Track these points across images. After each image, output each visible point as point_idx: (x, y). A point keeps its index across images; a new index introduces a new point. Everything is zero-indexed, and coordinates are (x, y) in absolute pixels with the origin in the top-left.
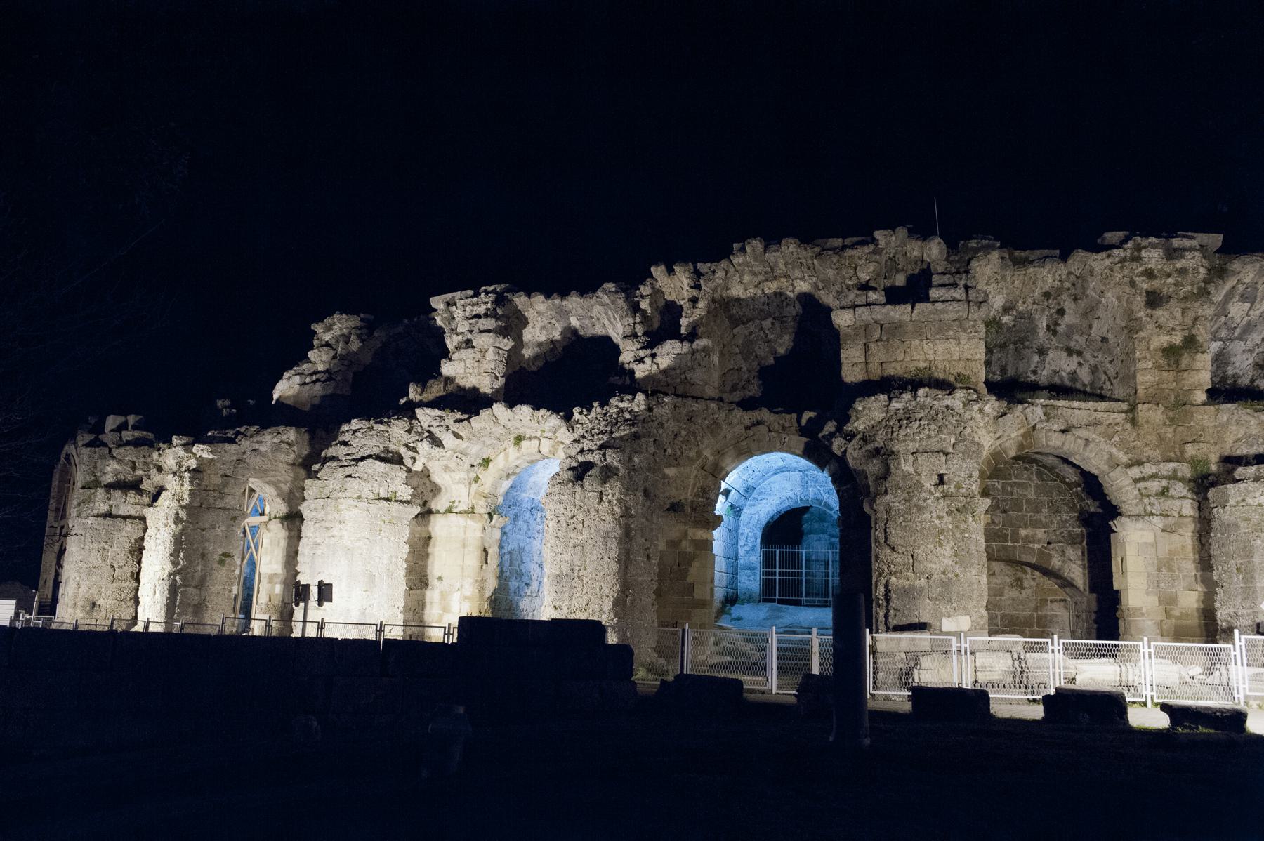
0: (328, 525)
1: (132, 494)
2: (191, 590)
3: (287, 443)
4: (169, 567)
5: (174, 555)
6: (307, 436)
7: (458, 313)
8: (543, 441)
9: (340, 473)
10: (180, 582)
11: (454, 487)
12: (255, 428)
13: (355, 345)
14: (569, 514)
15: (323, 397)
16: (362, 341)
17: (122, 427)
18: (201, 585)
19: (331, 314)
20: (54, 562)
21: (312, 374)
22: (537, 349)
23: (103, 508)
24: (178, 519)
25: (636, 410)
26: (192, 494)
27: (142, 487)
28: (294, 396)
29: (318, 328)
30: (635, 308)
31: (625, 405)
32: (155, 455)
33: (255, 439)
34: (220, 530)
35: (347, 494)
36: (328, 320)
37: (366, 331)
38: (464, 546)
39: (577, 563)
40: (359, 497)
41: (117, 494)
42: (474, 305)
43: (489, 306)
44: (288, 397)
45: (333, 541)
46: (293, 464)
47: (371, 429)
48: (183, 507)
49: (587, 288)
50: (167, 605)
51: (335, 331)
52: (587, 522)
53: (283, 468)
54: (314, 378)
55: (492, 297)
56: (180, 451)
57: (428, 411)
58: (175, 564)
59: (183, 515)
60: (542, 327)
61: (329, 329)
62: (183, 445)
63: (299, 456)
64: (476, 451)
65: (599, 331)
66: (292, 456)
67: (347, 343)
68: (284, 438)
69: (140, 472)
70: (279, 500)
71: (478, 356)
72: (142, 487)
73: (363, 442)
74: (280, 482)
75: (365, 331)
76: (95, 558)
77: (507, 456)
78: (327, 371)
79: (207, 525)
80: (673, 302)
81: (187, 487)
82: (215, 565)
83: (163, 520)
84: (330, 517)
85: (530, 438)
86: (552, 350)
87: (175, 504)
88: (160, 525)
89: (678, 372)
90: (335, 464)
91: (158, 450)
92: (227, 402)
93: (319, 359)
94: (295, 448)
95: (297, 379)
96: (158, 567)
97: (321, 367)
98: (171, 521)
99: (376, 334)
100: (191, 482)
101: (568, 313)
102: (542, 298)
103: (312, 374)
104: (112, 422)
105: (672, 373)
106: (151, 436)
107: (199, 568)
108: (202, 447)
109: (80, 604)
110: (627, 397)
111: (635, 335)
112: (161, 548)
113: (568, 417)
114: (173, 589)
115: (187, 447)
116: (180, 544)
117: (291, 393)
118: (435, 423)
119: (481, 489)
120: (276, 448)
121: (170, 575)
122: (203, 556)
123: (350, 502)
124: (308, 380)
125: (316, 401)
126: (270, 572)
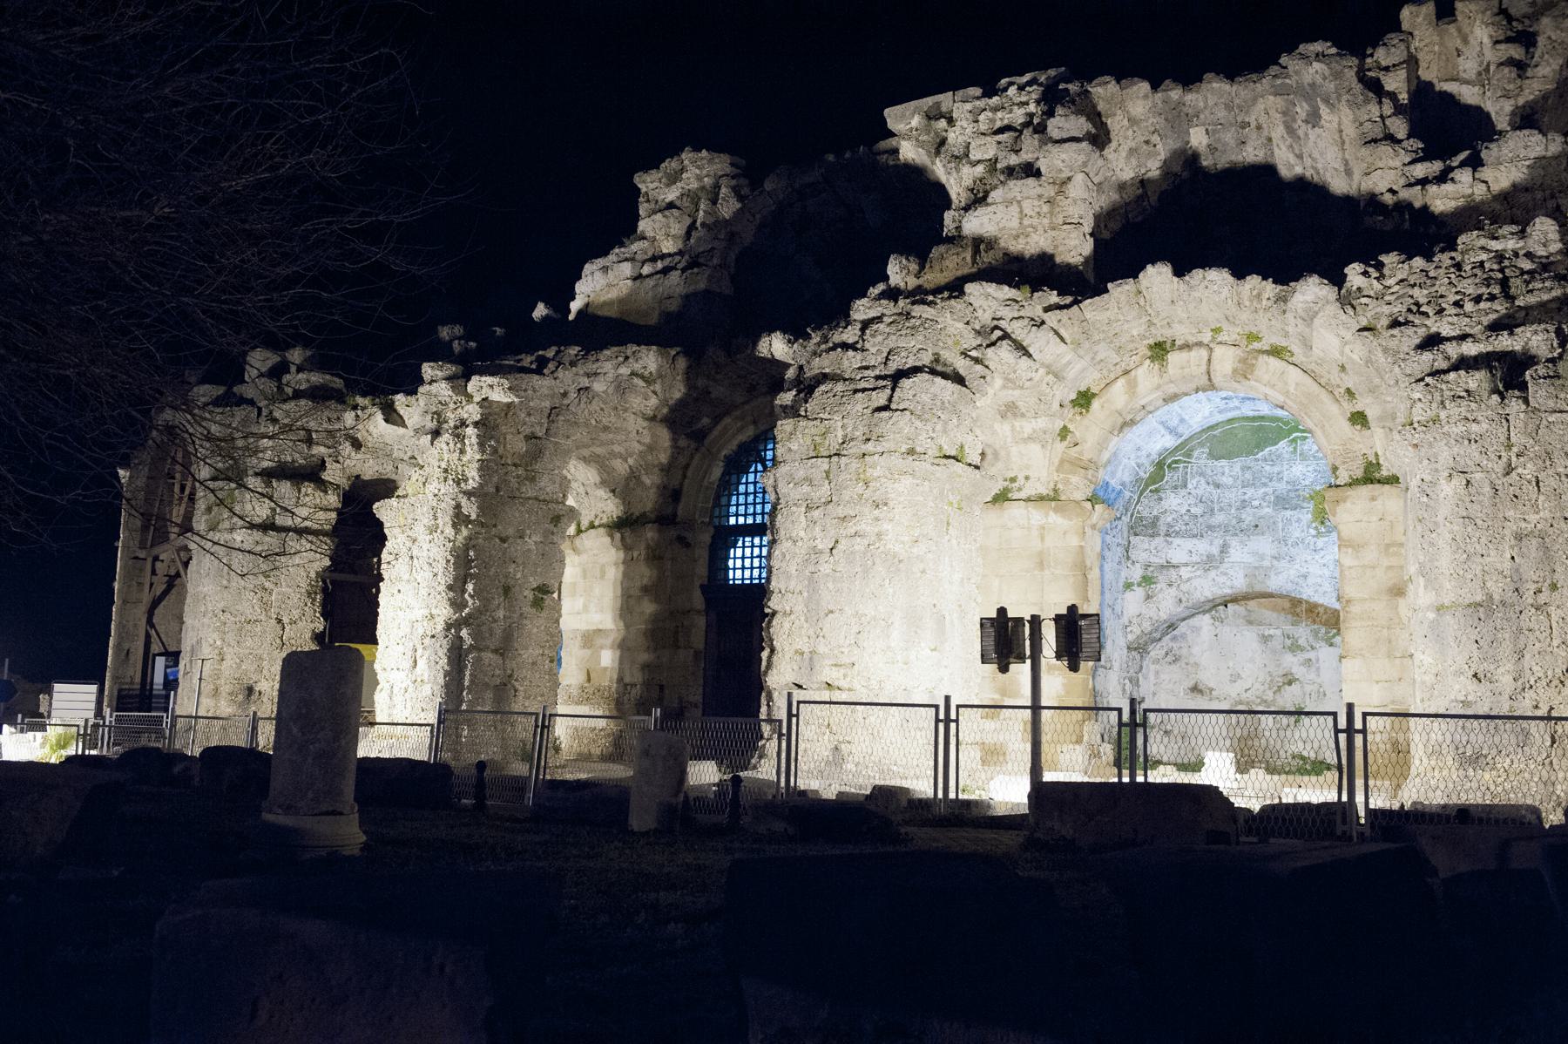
0: (840, 512)
1: (308, 488)
2: (488, 656)
3: (642, 377)
4: (444, 612)
5: (456, 587)
6: (682, 363)
7: (946, 136)
8: (1219, 351)
9: (860, 404)
10: (468, 641)
11: (1014, 450)
12: (573, 351)
13: (728, 207)
14: (1499, 467)
15: (687, 297)
16: (741, 198)
17: (277, 372)
18: (504, 649)
19: (675, 152)
20: (144, 621)
21: (654, 259)
22: (1115, 196)
23: (261, 511)
24: (459, 519)
25: (1541, 252)
26: (484, 467)
27: (326, 476)
28: (621, 301)
29: (647, 183)
30: (1375, 88)
31: (1511, 244)
32: (349, 418)
33: (580, 369)
34: (533, 540)
35: (885, 445)
36: (670, 165)
37: (749, 176)
38: (1041, 565)
39: (1530, 574)
40: (911, 452)
41: (284, 489)
42: (995, 109)
43: (1032, 108)
44: (605, 304)
45: (859, 545)
46: (653, 419)
47: (908, 316)
48: (469, 494)
49: (1248, 55)
50: (447, 685)
51: (677, 198)
52: (1549, 482)
53: (635, 424)
54: (660, 265)
55: (1035, 92)
56: (443, 390)
57: (991, 288)
58: (457, 605)
59: (470, 509)
60: (1132, 151)
61: (674, 178)
62: (448, 379)
63: (664, 402)
64: (1082, 374)
65: (1252, 154)
66: (653, 401)
67: (714, 202)
68: (637, 367)
69: (320, 450)
70: (602, 493)
71: (1050, 191)
72: (326, 476)
73: (892, 342)
74: (613, 455)
75: (743, 181)
76: (249, 606)
77: (1132, 387)
78: (680, 253)
79: (511, 531)
80: (1430, 84)
81: (473, 454)
82: (527, 609)
83: (427, 520)
84: (846, 495)
85: (1186, 346)
86: (1140, 199)
87: (449, 488)
88: (420, 531)
89: (1539, 195)
90: (840, 387)
91: (355, 408)
92: (458, 330)
93: (660, 232)
94: (658, 387)
95: (627, 269)
96: (419, 613)
97: (668, 247)
98: (445, 522)
99: (768, 185)
100: (481, 445)
101: (1190, 119)
102: (1145, 86)
103: (654, 259)
104: (259, 360)
105: (1524, 198)
106: (338, 383)
107: (501, 614)
108: (489, 380)
109: (225, 689)
110: (1507, 229)
111: (1391, 138)
112: (424, 576)
113: (1338, 280)
114: (457, 655)
115: (459, 381)
116: (468, 566)
117: (613, 294)
118: (1007, 313)
119: (1073, 452)
120: (622, 388)
121: (448, 627)
122: (507, 590)
123: (896, 461)
124: (646, 270)
125: (673, 306)
126: (584, 627)
